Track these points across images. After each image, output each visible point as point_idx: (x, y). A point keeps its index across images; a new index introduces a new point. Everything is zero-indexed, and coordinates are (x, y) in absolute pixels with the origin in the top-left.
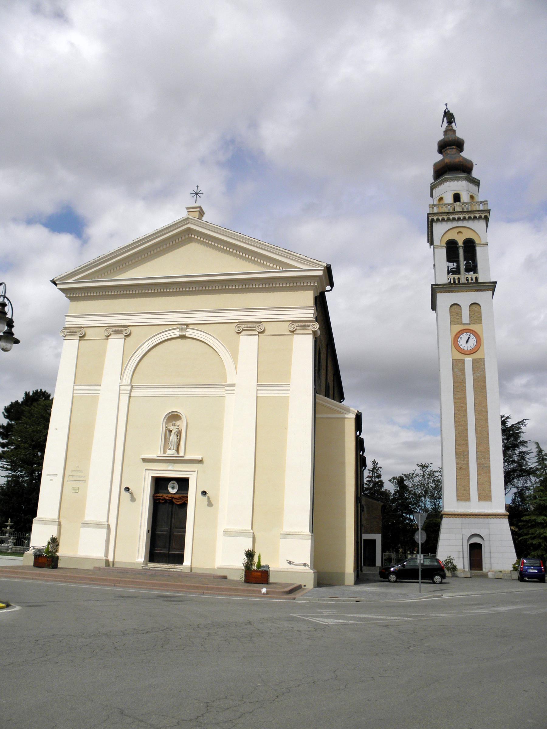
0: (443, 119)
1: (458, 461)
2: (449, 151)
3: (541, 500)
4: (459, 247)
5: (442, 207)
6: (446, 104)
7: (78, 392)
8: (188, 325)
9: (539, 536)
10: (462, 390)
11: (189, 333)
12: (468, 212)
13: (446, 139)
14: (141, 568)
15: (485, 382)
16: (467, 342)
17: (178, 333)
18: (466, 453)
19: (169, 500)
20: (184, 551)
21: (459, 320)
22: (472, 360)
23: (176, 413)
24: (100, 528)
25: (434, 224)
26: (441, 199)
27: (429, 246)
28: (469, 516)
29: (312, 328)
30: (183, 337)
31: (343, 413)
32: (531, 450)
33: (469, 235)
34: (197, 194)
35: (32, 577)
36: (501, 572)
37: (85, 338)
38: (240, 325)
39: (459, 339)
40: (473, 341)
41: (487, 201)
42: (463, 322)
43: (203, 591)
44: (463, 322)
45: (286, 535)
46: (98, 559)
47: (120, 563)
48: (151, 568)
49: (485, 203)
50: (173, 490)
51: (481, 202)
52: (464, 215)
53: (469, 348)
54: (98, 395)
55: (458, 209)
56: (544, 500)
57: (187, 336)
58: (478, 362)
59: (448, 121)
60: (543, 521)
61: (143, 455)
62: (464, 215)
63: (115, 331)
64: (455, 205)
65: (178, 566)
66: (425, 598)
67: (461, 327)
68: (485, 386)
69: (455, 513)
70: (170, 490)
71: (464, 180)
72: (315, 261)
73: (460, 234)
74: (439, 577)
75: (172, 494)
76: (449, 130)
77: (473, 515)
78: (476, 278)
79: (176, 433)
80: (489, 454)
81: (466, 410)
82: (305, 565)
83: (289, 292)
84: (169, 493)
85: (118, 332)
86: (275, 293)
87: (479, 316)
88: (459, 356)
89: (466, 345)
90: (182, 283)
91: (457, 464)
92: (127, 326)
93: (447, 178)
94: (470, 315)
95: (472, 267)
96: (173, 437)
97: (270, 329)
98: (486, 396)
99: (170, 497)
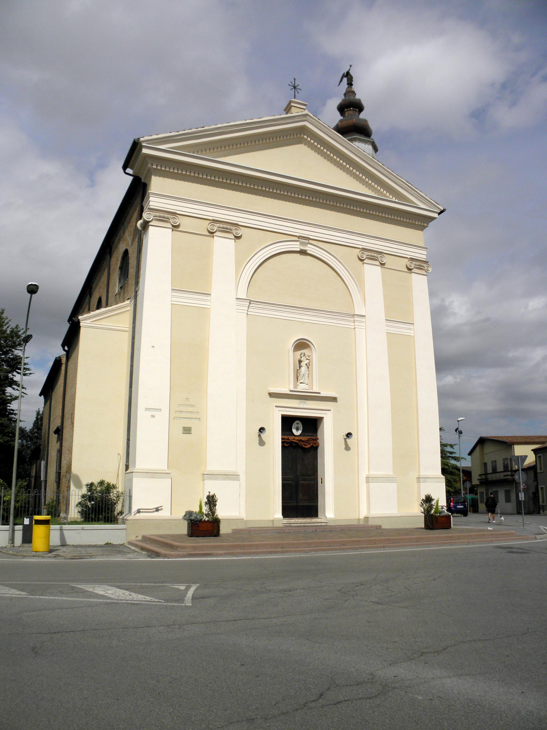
11: (310, 249)
14: (282, 525)
17: (299, 246)
20: (318, 503)
24: (230, 479)
29: (171, 221)
30: (303, 252)
35: (382, 545)
38: (363, 252)
43: (468, 540)
46: (236, 520)
48: (293, 525)
54: (209, 307)
57: (308, 252)
65: (314, 520)
70: (294, 431)
72: (433, 202)
75: (295, 436)
83: (242, 193)
86: (265, 198)
90: (197, 166)
92: (237, 225)
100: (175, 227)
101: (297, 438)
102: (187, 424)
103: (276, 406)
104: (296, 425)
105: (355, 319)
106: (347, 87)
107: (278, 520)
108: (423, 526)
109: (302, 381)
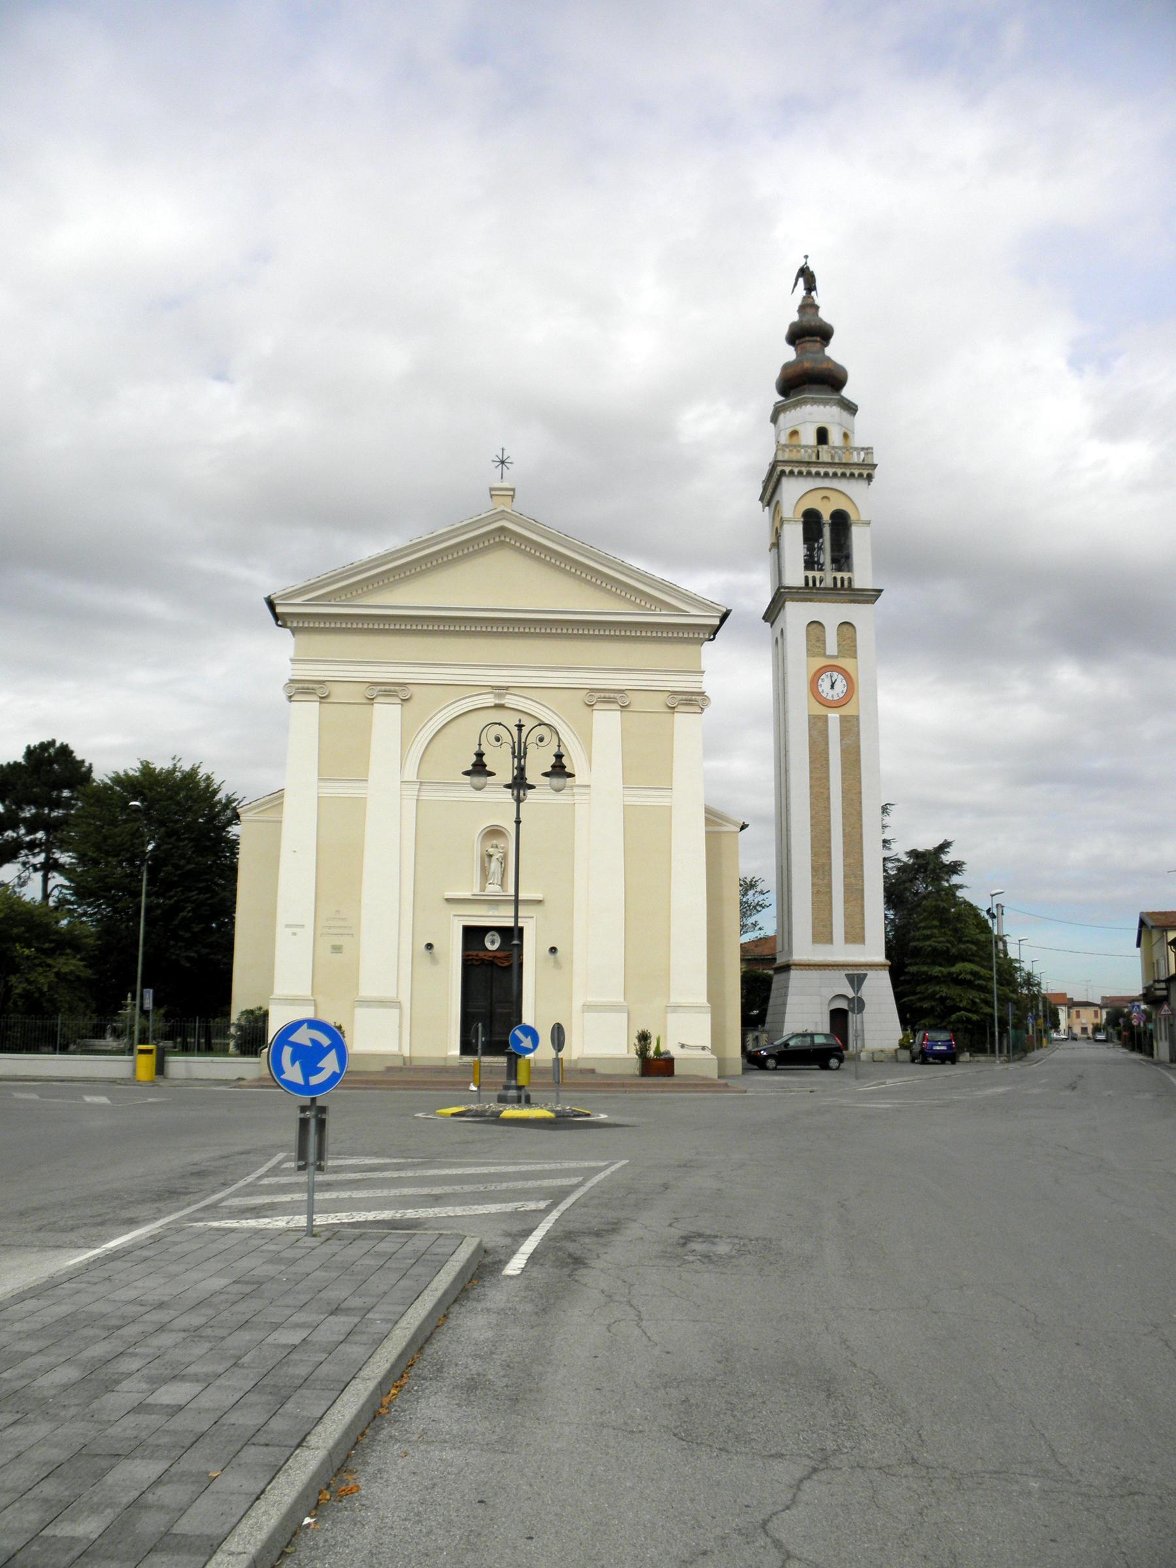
0: (797, 280)
1: (815, 880)
2: (808, 345)
3: (936, 942)
4: (824, 524)
5: (798, 451)
6: (806, 257)
7: (325, 791)
8: (508, 688)
9: (932, 997)
10: (822, 765)
11: (509, 701)
12: (840, 464)
13: (805, 323)
14: (458, 1064)
15: (858, 753)
16: (832, 687)
17: (493, 700)
18: (827, 868)
19: (488, 961)
21: (820, 650)
22: (841, 716)
23: (499, 828)
24: (387, 1007)
25: (784, 480)
26: (794, 433)
27: (762, 508)
28: (830, 968)
31: (720, 825)
32: (896, 855)
33: (842, 505)
34: (503, 462)
36: (882, 1051)
37: (329, 700)
39: (820, 680)
40: (841, 686)
41: (872, 448)
42: (827, 654)
44: (827, 654)
45: (677, 1008)
47: (418, 1058)
49: (869, 451)
50: (492, 944)
51: (863, 449)
52: (834, 470)
53: (836, 698)
55: (825, 457)
56: (939, 942)
57: (507, 705)
58: (849, 721)
59: (808, 286)
60: (940, 975)
61: (446, 893)
62: (834, 470)
63: (385, 691)
64: (820, 450)
66: (873, 1086)
67: (822, 662)
68: (858, 761)
69: (811, 963)
71: (835, 405)
73: (825, 500)
74: (836, 1061)
75: (491, 951)
76: (808, 306)
77: (809, 965)
78: (850, 580)
79: (500, 859)
80: (862, 871)
81: (828, 798)
82: (703, 1048)
84: (486, 949)
85: (388, 694)
87: (852, 644)
88: (820, 710)
89: (831, 692)
91: (813, 885)
93: (808, 398)
94: (838, 641)
95: (842, 559)
96: (494, 866)
97: (638, 702)
98: (860, 778)
99: (490, 957)
100: (323, 699)
101: (490, 954)
102: (337, 941)
103: (455, 915)
104: (491, 937)
105: (575, 791)
106: (804, 295)
107: (453, 1057)
108: (637, 1073)
109: (491, 881)
